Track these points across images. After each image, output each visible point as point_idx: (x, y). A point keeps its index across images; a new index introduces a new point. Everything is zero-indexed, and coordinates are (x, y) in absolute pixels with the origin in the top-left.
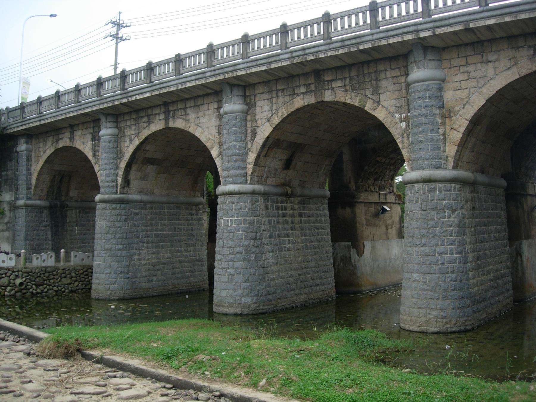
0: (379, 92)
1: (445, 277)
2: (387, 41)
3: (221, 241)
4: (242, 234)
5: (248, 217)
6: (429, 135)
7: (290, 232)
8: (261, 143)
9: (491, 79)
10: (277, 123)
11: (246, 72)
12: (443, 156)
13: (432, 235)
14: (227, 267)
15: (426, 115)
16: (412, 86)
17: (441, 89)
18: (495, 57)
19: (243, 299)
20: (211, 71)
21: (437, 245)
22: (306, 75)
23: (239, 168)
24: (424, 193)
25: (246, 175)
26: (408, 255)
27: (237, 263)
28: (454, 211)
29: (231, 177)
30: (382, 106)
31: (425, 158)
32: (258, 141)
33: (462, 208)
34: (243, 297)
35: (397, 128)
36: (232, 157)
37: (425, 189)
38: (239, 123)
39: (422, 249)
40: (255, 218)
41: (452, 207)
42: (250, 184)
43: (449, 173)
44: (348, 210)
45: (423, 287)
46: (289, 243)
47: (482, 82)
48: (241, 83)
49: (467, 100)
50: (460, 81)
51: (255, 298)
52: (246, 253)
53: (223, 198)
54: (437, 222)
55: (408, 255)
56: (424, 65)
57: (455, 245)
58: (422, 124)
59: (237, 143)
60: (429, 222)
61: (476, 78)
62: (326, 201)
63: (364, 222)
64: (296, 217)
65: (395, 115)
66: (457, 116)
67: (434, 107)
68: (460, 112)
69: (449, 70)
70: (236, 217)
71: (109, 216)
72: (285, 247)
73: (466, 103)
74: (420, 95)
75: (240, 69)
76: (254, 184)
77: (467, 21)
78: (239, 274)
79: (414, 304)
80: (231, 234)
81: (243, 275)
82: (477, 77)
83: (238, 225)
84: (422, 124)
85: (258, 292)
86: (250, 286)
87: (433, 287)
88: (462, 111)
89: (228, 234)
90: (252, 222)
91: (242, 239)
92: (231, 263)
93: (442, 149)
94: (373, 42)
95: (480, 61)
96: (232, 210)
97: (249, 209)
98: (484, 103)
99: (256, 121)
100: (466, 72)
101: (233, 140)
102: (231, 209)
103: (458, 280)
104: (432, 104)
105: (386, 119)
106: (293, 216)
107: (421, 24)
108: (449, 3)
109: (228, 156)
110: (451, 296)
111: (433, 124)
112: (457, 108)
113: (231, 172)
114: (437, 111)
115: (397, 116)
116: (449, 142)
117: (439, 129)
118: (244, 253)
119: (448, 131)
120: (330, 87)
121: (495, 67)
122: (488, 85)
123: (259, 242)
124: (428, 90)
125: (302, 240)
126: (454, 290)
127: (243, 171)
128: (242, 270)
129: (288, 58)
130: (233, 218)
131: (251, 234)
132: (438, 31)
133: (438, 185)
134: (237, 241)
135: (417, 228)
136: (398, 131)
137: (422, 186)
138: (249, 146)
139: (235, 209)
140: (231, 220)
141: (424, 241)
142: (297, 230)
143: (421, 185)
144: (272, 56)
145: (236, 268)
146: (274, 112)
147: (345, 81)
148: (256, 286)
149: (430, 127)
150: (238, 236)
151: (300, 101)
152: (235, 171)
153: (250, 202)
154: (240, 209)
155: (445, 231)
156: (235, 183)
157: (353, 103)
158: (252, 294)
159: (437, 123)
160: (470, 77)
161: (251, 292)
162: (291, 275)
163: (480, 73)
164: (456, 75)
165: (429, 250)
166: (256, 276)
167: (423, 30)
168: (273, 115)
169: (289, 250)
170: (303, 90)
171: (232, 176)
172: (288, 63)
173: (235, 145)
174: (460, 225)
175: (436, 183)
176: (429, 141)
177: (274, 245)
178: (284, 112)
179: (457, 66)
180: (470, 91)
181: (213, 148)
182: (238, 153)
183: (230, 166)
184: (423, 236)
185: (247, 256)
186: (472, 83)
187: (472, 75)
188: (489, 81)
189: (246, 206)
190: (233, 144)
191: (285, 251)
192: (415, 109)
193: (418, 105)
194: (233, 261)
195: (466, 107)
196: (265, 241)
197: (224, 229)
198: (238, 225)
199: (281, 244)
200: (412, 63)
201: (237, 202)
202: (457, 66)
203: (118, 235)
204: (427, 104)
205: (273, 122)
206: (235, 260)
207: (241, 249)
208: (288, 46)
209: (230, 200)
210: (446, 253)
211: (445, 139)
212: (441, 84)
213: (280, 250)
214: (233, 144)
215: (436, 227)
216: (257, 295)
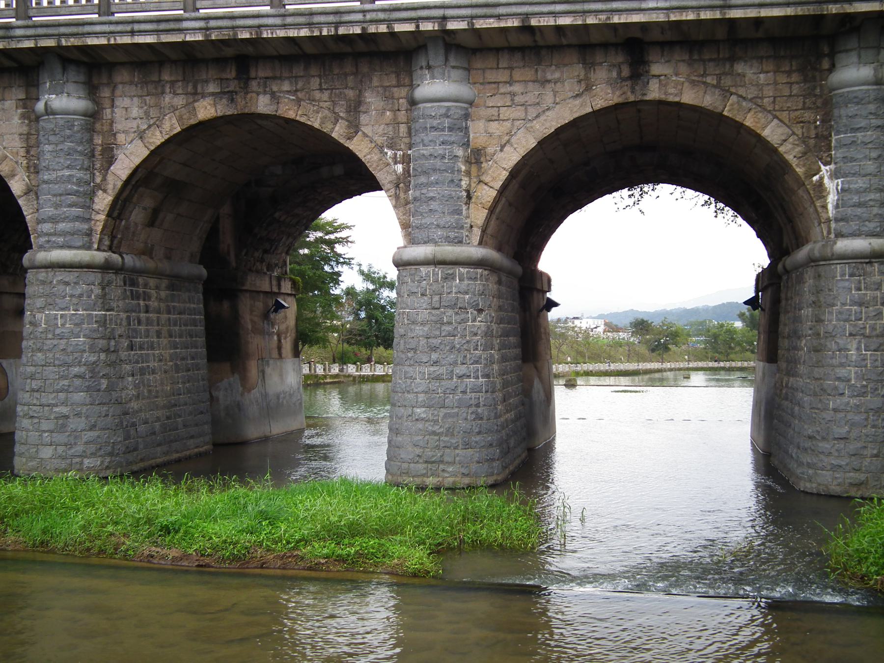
0: (360, 109)
1: (467, 413)
2: (377, 28)
3: (39, 354)
4: (84, 343)
5: (95, 310)
6: (446, 190)
7: (155, 340)
8: (124, 177)
9: (548, 109)
10: (159, 143)
11: (109, 40)
12: (466, 223)
13: (448, 348)
14: (53, 402)
15: (443, 157)
16: (421, 106)
17: (467, 116)
18: (557, 75)
21: (455, 363)
22: (221, 62)
23: (77, 218)
24: (437, 281)
25: (89, 233)
26: (406, 378)
27: (75, 394)
28: (480, 311)
29: (60, 235)
30: (364, 133)
31: (438, 226)
32: (119, 173)
33: (490, 306)
34: (86, 457)
35: (388, 172)
36: (63, 198)
37: (438, 274)
38: (79, 134)
39: (432, 369)
40: (108, 313)
41: (478, 305)
42: (98, 249)
43: (475, 251)
44: (226, 305)
45: (433, 429)
46: (154, 361)
47: (532, 112)
48: (85, 59)
49: (507, 138)
50: (499, 107)
51: (108, 459)
52: (91, 377)
53: (44, 274)
54: (456, 328)
55: (406, 378)
56: (444, 74)
57: (481, 364)
58: (434, 170)
59: (74, 172)
60: (444, 328)
61: (523, 105)
62: (201, 287)
63: (250, 327)
64: (163, 314)
65: (386, 150)
66: (490, 163)
67: (456, 145)
68: (495, 157)
69: (481, 87)
70: (73, 310)
72: (148, 366)
73: (506, 144)
74: (435, 123)
75: (96, 34)
76: (104, 251)
77: (527, 15)
78: (78, 415)
79: (418, 456)
80: (63, 342)
81: (87, 417)
82: (527, 104)
83: (76, 325)
84: (434, 170)
85: (113, 447)
86: (98, 437)
87: (450, 428)
88: (500, 155)
89: (55, 342)
90: (103, 320)
91: (84, 351)
92: (62, 396)
93: (464, 212)
94: (365, 25)
95: (532, 79)
96: (64, 297)
97: (97, 296)
98: (534, 145)
99: (115, 135)
100: (510, 93)
101: (66, 165)
102: (63, 294)
103: (485, 418)
104: (453, 139)
105: (369, 157)
106: (158, 312)
107: (268, 16)
108: (58, 2)
109: (55, 195)
110: (476, 442)
111: (453, 172)
112: (490, 150)
113: (62, 226)
114: (460, 152)
115: (390, 153)
116: (476, 203)
117: (461, 180)
118: (87, 377)
119: (473, 185)
120: (268, 89)
121: (557, 90)
122: (542, 118)
123: (113, 357)
124: (448, 117)
125: (171, 355)
126: (479, 433)
127: (85, 226)
129: (200, 29)
130: (67, 312)
131: (101, 341)
132: (480, 24)
133: (459, 270)
134: (76, 355)
135: (422, 336)
136: (389, 178)
137: (434, 271)
138: (98, 180)
139: (72, 296)
140: (62, 316)
141: (434, 356)
142: (165, 338)
143: (431, 269)
144: (167, 20)
145: (72, 404)
146: (152, 122)
147: (297, 84)
148: (108, 437)
149: (448, 175)
150: (77, 345)
151: (209, 107)
152: (70, 225)
153: (99, 284)
154: (81, 296)
155: (468, 342)
156: (70, 247)
157: (309, 123)
158: (102, 452)
159: (459, 171)
160: (516, 101)
161: (100, 449)
162: (157, 417)
163: (531, 98)
164: (491, 96)
165: (442, 370)
166: (109, 419)
167: (453, 18)
168: (150, 126)
169: (154, 372)
170: (212, 88)
171: (64, 234)
172: (199, 37)
173: (70, 175)
174: (488, 334)
175: (456, 266)
176: (446, 199)
177: (134, 363)
178: (172, 126)
179: (495, 83)
180: (513, 125)
181: (13, 176)
182: (77, 191)
183: (59, 215)
184: (434, 349)
185: (95, 381)
186: (519, 113)
187: (518, 99)
188: (544, 111)
189: (92, 290)
190: (67, 173)
191: (149, 374)
192: (424, 145)
193: (430, 138)
194: (67, 391)
195: (506, 149)
196: (123, 355)
197: (46, 331)
198: (76, 325)
199: (143, 362)
200: (421, 68)
201: (75, 283)
202: (495, 83)
204: (446, 138)
205: (151, 141)
206: (71, 390)
207: (83, 369)
208: (113, 9)
209: (60, 278)
210: (469, 377)
211: (469, 197)
212: (467, 109)
213: (142, 372)
214: (67, 173)
215: (454, 336)
216: (111, 454)
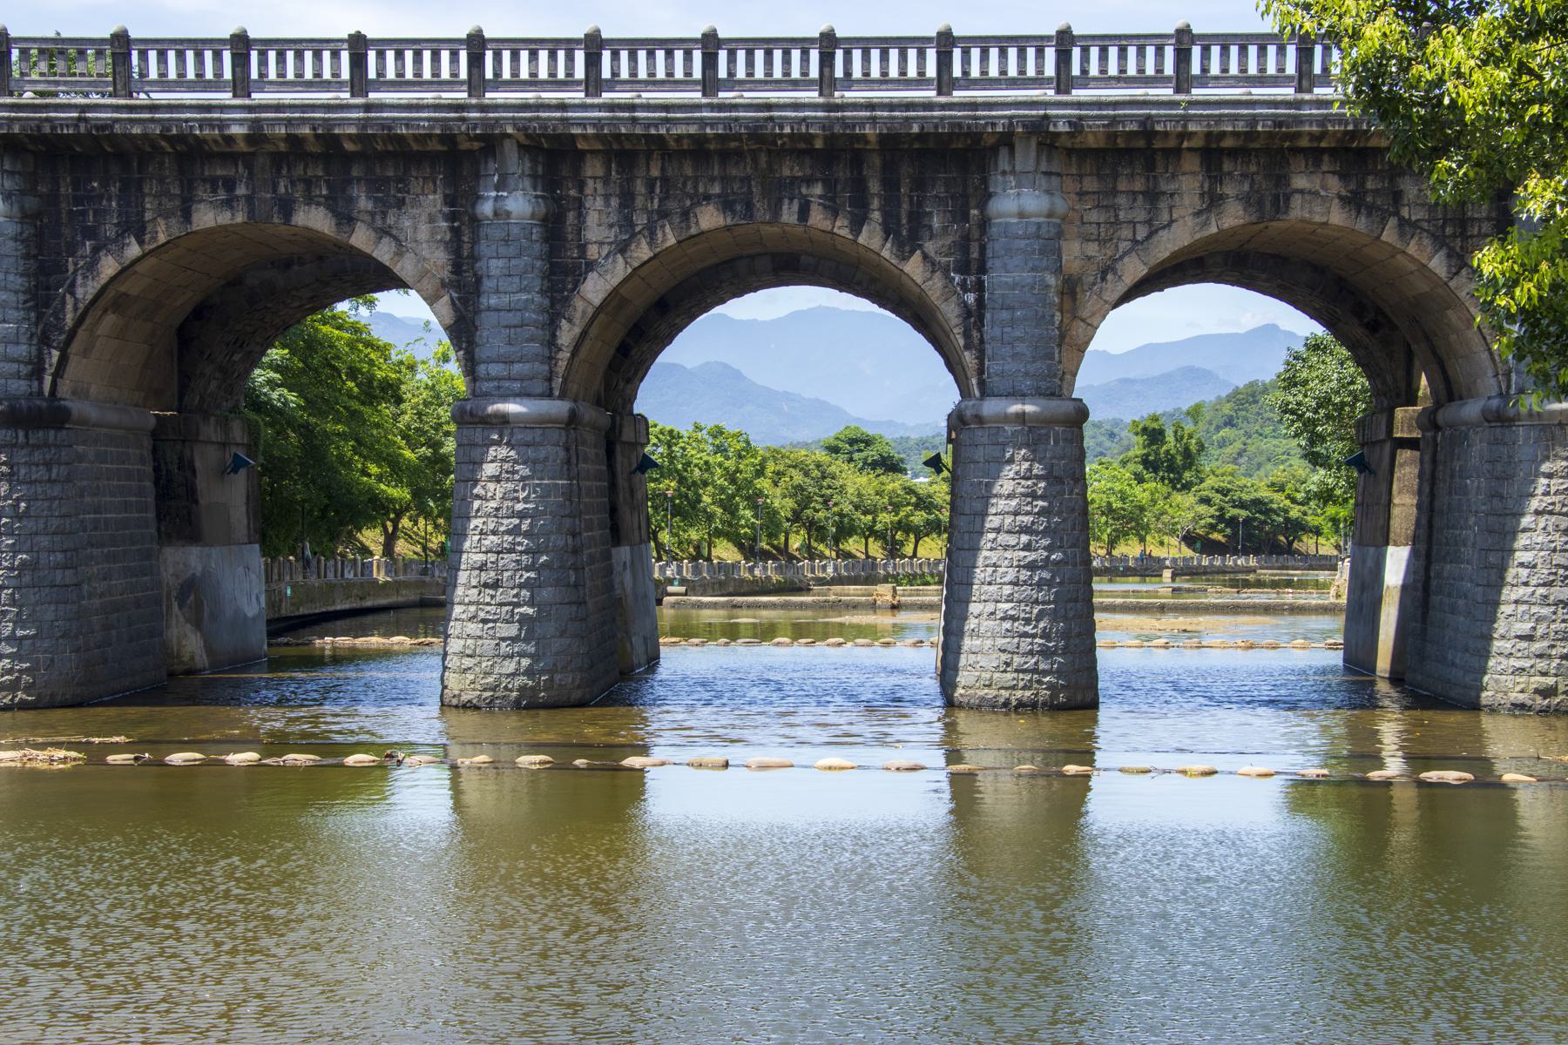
19: (557, 677)
20: (49, 82)
71: (26, 463)
93: (1057, 356)
113: (517, 368)
128: (554, 608)
152: (528, 366)
154: (546, 459)
203: (54, 523)
211: (1062, 336)
